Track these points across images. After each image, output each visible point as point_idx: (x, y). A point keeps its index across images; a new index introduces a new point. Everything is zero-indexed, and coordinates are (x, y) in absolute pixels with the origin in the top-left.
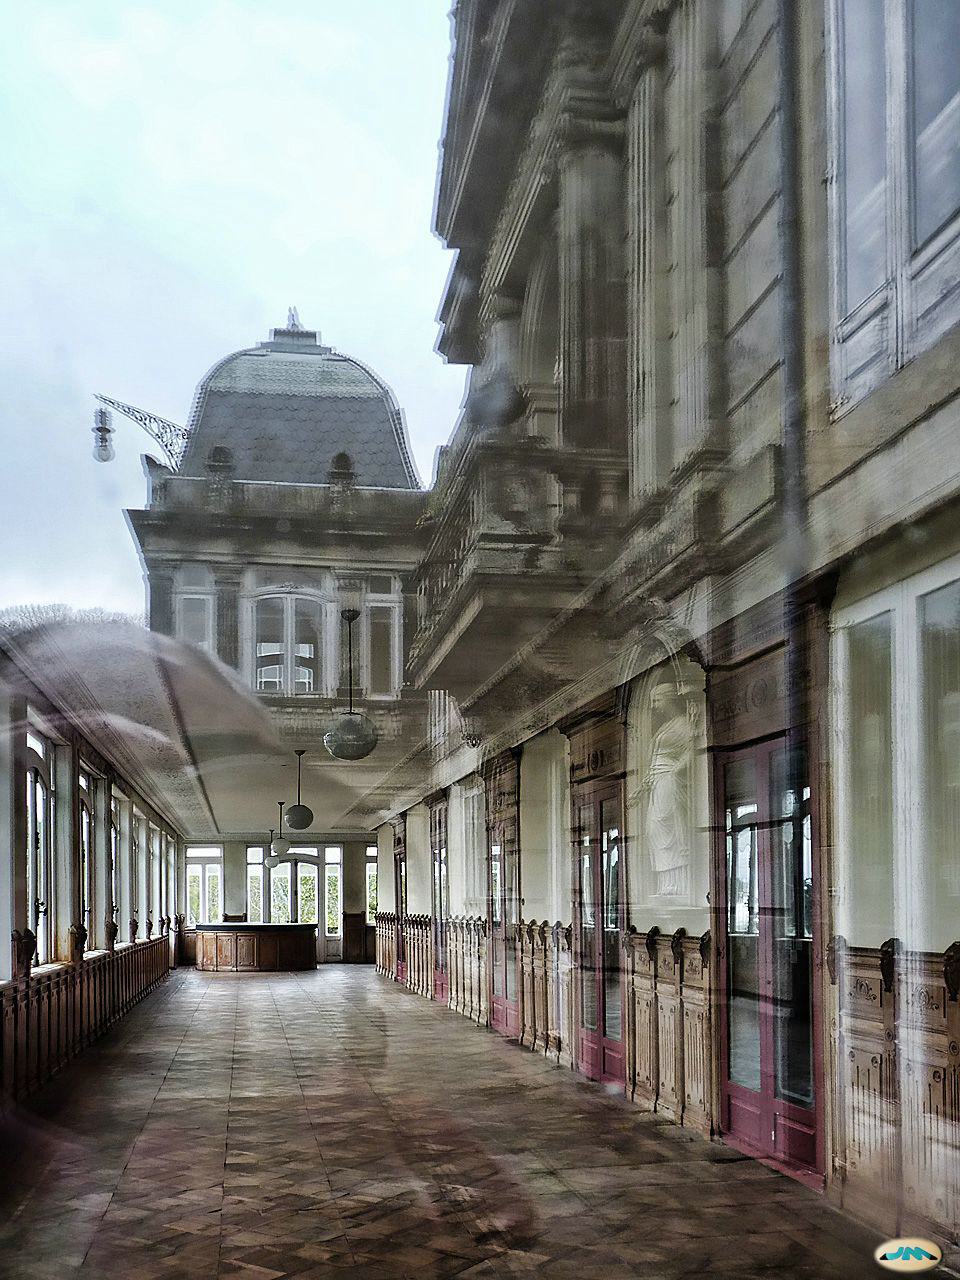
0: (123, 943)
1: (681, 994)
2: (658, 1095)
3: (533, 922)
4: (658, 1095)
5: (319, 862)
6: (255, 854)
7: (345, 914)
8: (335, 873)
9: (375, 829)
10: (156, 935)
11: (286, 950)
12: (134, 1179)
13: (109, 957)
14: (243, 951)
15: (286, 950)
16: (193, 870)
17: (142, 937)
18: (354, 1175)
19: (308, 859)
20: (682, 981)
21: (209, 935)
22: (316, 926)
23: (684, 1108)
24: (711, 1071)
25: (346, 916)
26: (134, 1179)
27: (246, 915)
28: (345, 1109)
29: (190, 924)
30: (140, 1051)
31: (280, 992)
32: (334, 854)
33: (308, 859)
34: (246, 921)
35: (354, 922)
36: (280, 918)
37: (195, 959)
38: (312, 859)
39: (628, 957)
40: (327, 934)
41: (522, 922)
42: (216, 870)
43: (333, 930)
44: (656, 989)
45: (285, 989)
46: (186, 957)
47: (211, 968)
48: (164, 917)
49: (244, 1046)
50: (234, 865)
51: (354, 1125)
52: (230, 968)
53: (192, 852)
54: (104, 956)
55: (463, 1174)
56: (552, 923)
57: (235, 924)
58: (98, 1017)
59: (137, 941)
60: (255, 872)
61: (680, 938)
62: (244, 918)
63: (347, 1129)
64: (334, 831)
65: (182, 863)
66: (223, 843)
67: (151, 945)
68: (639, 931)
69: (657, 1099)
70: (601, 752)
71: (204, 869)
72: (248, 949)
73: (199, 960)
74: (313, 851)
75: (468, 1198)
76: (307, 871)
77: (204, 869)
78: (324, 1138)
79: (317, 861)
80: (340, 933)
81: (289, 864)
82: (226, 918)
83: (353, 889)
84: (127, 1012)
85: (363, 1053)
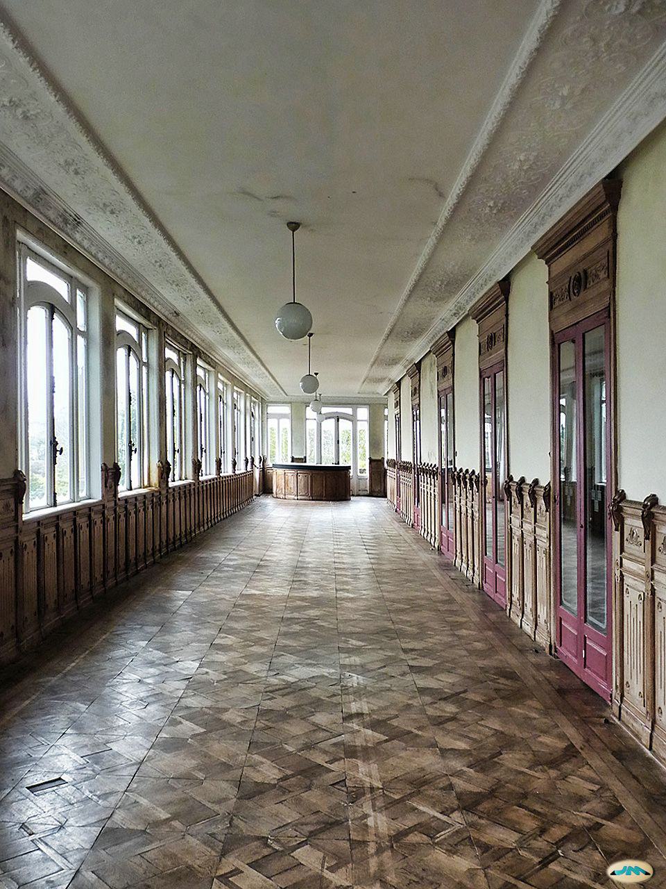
0: (208, 473)
1: (535, 533)
2: (523, 613)
3: (523, 480)
4: (523, 613)
5: (353, 419)
6: (310, 413)
7: (370, 459)
8: (363, 427)
9: (386, 395)
10: (241, 469)
11: (330, 484)
12: (150, 649)
13: (194, 485)
14: (301, 484)
15: (330, 484)
16: (272, 423)
17: (227, 471)
18: (289, 659)
19: (346, 417)
20: (535, 521)
21: (280, 471)
22: (349, 467)
23: (536, 625)
24: (550, 596)
25: (371, 461)
26: (150, 649)
27: (305, 457)
28: (310, 608)
29: (269, 463)
30: (204, 555)
31: (315, 516)
32: (363, 413)
33: (346, 417)
34: (305, 462)
35: (377, 468)
36: (328, 461)
37: (272, 489)
38: (347, 417)
39: (508, 500)
40: (359, 474)
41: (511, 478)
42: (286, 423)
43: (362, 471)
44: (522, 527)
45: (326, 515)
46: (266, 489)
47: (282, 496)
48: (249, 458)
49: (270, 556)
50: (298, 420)
51: (310, 621)
52: (293, 497)
53: (272, 409)
54: (190, 485)
55: (362, 666)
56: (529, 481)
57: (297, 465)
58: (183, 530)
59: (237, 472)
60: (311, 426)
61: (521, 484)
62: (304, 460)
63: (303, 624)
64: (359, 395)
65: (264, 416)
66: (291, 403)
67: (245, 475)
68: (514, 480)
69: (522, 617)
70: (494, 334)
71: (279, 423)
72: (304, 484)
73: (274, 491)
74: (349, 411)
75: (355, 685)
76: (345, 425)
77: (279, 423)
78: (284, 629)
79: (351, 417)
80: (367, 475)
81: (333, 420)
82: (293, 460)
83: (376, 442)
84: (212, 526)
85: (345, 566)
